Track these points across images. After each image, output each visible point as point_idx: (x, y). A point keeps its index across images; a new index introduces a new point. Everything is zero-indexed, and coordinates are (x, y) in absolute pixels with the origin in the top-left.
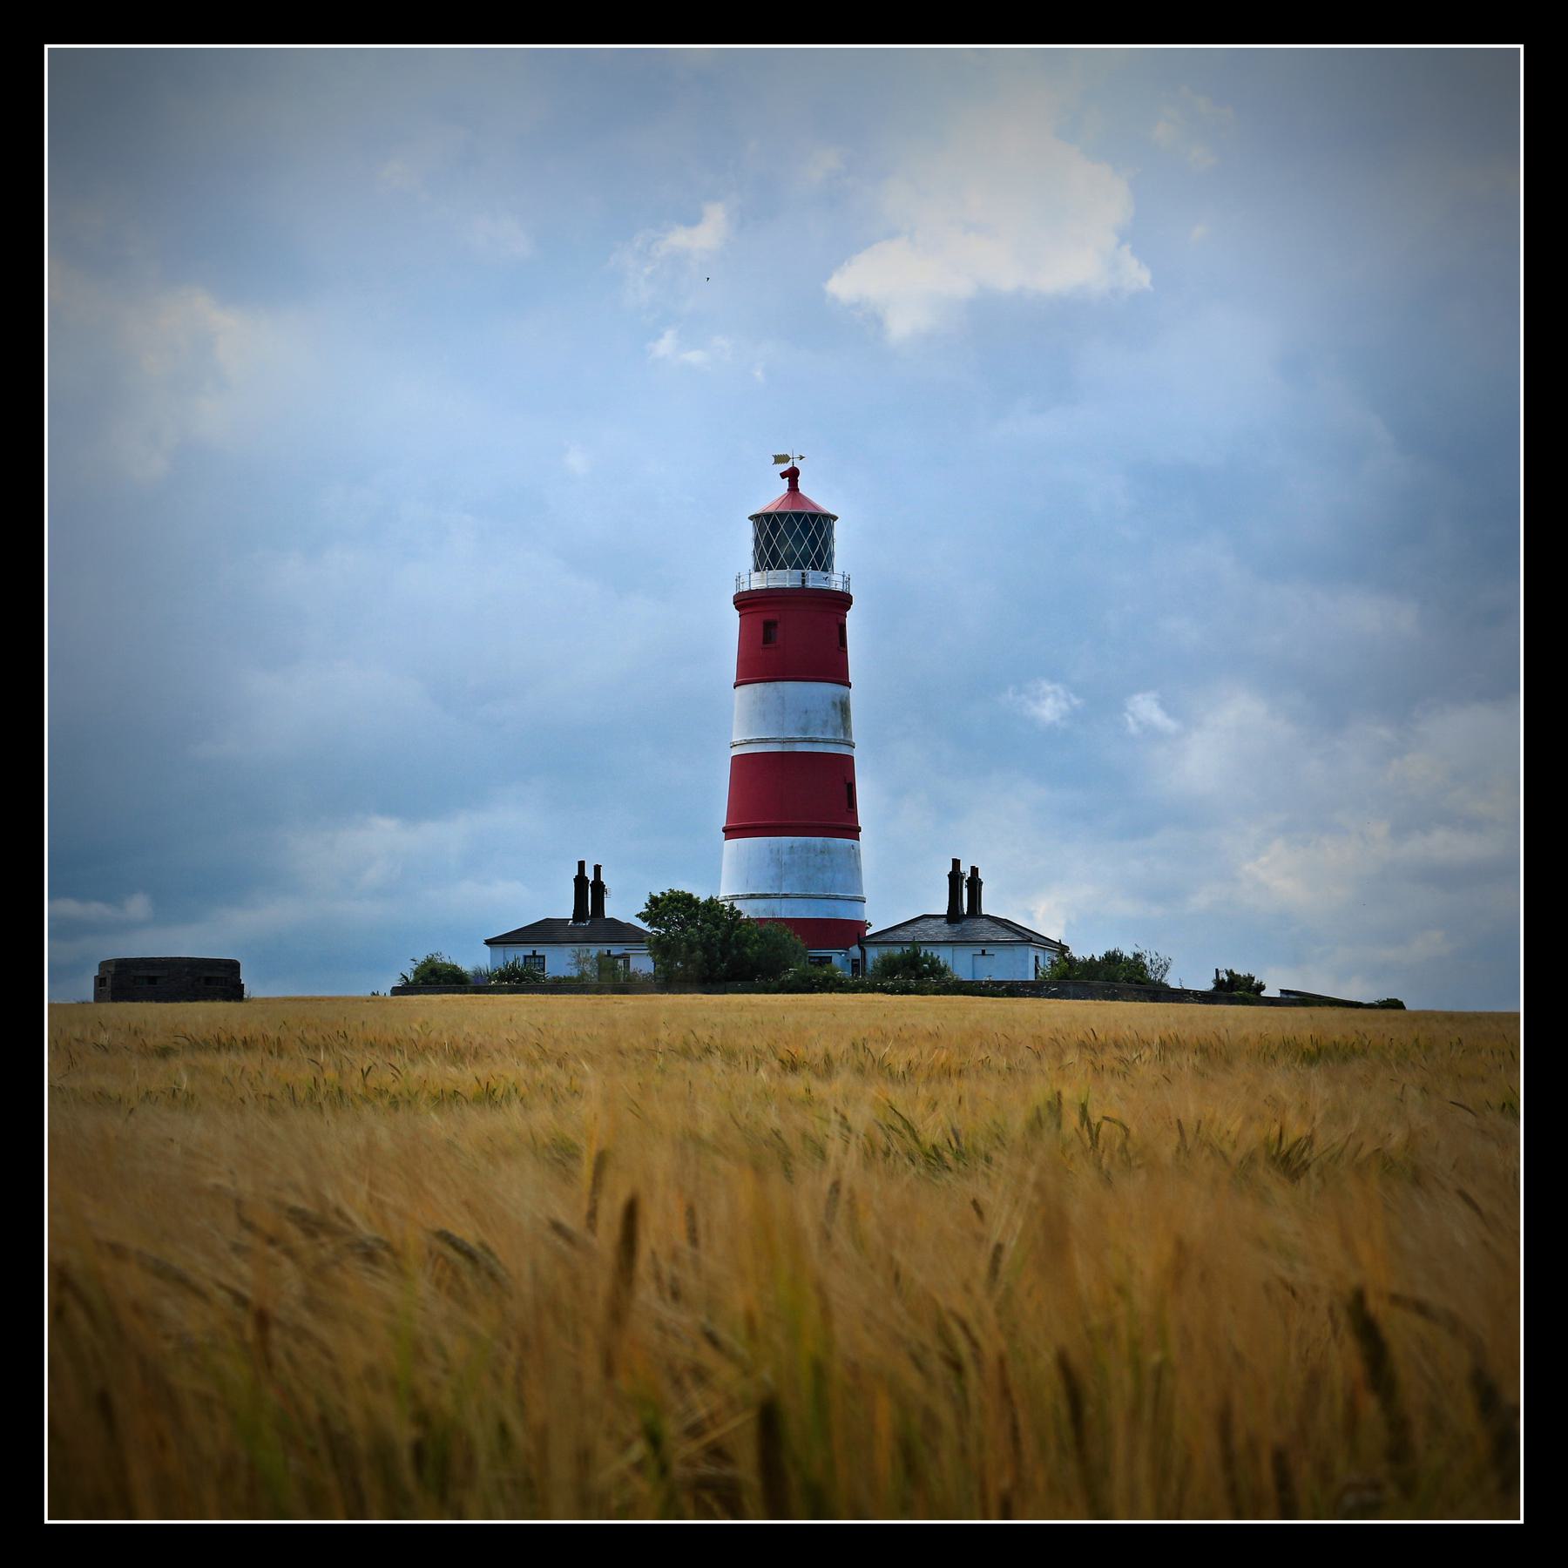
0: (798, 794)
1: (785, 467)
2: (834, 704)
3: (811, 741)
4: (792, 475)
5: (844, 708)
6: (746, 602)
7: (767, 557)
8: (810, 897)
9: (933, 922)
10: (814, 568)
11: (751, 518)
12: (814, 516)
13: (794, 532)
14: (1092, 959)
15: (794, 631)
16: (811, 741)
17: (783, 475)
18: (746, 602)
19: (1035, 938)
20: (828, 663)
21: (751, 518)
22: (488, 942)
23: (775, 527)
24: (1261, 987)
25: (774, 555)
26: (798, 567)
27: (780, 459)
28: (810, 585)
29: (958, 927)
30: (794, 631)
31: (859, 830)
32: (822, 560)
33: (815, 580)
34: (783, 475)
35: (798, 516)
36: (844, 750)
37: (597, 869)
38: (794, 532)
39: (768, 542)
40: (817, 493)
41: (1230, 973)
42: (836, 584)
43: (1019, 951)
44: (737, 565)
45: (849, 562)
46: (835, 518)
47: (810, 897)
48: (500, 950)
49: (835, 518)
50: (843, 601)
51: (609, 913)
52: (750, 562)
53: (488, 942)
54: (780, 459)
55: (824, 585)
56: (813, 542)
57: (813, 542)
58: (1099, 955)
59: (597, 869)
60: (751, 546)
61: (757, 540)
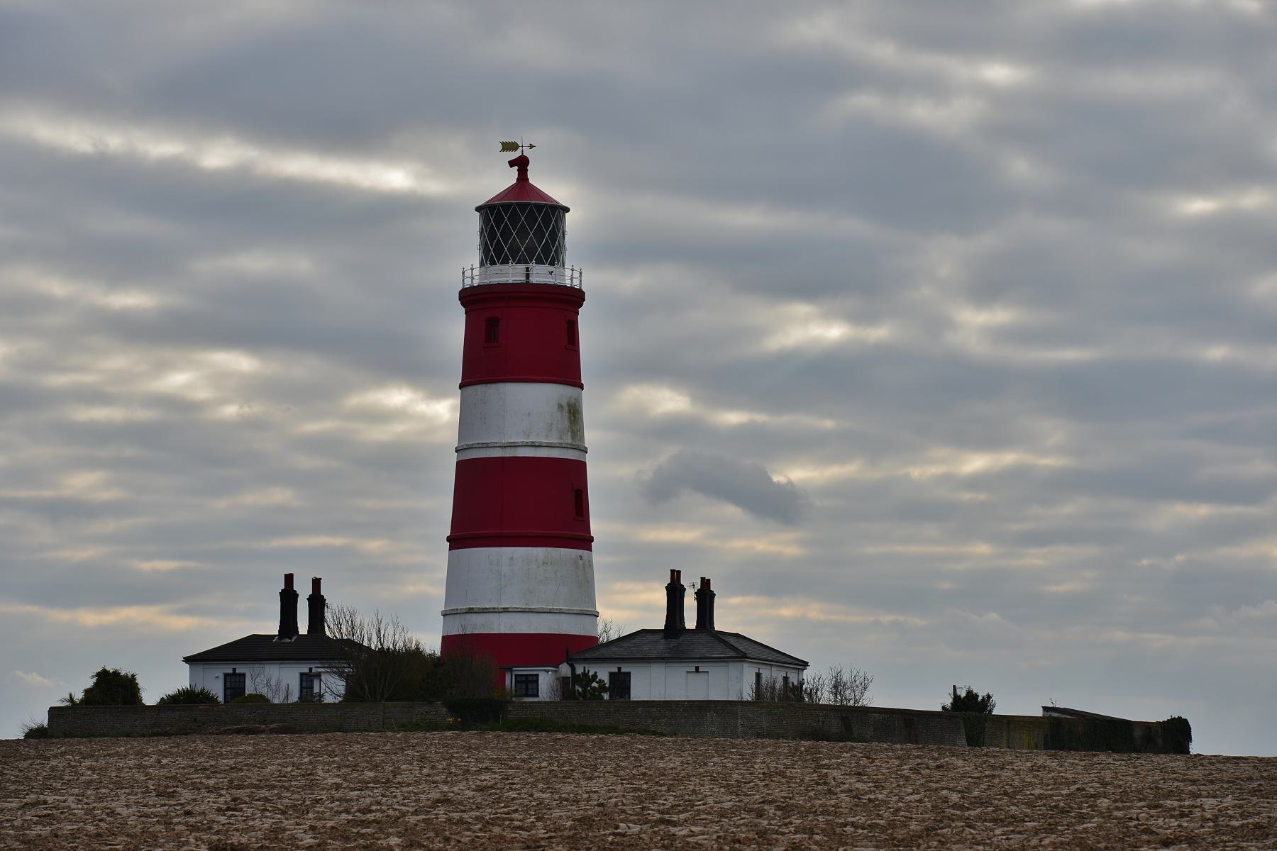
0: (517, 501)
1: (514, 155)
2: (560, 406)
3: (533, 445)
4: (521, 164)
5: (574, 413)
6: (470, 297)
7: (493, 251)
8: (531, 611)
9: (650, 637)
10: (539, 262)
11: (478, 209)
12: (540, 207)
13: (520, 222)
16: (533, 445)
17: (512, 164)
18: (470, 297)
19: (751, 651)
20: (561, 366)
21: (478, 209)
22: (188, 660)
23: (499, 220)
25: (499, 250)
27: (508, 147)
28: (534, 280)
29: (674, 643)
31: (591, 539)
32: (551, 252)
33: (541, 274)
34: (512, 164)
35: (523, 207)
38: (520, 222)
39: (492, 235)
41: (970, 693)
42: (567, 277)
43: (733, 669)
44: (465, 263)
46: (567, 210)
47: (531, 611)
48: (199, 668)
49: (567, 210)
50: (575, 297)
51: (721, 623)
52: (474, 258)
53: (188, 660)
54: (508, 147)
55: (549, 280)
56: (539, 234)
57: (539, 234)
58: (90, 683)
61: (481, 232)
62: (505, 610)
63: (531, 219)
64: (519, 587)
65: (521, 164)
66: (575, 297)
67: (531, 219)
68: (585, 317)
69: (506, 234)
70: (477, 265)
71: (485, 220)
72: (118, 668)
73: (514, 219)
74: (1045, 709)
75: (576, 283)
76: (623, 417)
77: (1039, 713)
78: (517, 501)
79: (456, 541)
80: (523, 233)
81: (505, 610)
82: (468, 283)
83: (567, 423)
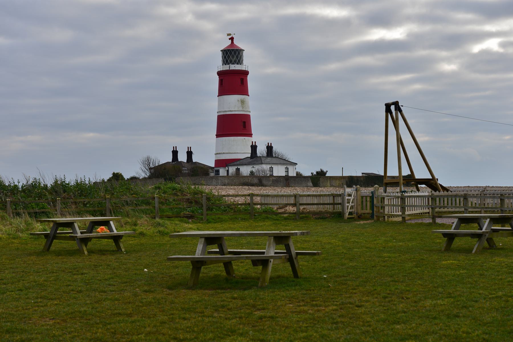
0: (233, 125)
1: (230, 37)
2: (238, 100)
3: (230, 111)
4: (232, 39)
12: (237, 50)
13: (232, 54)
14: (103, 180)
15: (233, 81)
16: (230, 111)
17: (230, 39)
18: (220, 73)
24: (325, 173)
25: (227, 61)
26: (229, 64)
30: (233, 81)
32: (239, 61)
34: (230, 39)
35: (233, 50)
36: (248, 113)
37: (190, 154)
38: (232, 54)
39: (225, 57)
40: (239, 44)
44: (219, 65)
45: (249, 62)
47: (230, 153)
50: (246, 73)
52: (221, 63)
54: (229, 35)
55: (240, 69)
56: (237, 57)
57: (237, 57)
59: (190, 154)
60: (221, 59)
62: (224, 153)
63: (235, 53)
64: (238, 147)
65: (232, 39)
66: (246, 73)
67: (231, 53)
68: (250, 78)
69: (229, 57)
70: (221, 65)
71: (223, 54)
72: (60, 176)
73: (231, 53)
74: (362, 173)
75: (247, 70)
76: (252, 103)
77: (361, 175)
78: (233, 125)
79: (218, 136)
80: (233, 57)
81: (224, 153)
82: (219, 70)
83: (240, 105)
